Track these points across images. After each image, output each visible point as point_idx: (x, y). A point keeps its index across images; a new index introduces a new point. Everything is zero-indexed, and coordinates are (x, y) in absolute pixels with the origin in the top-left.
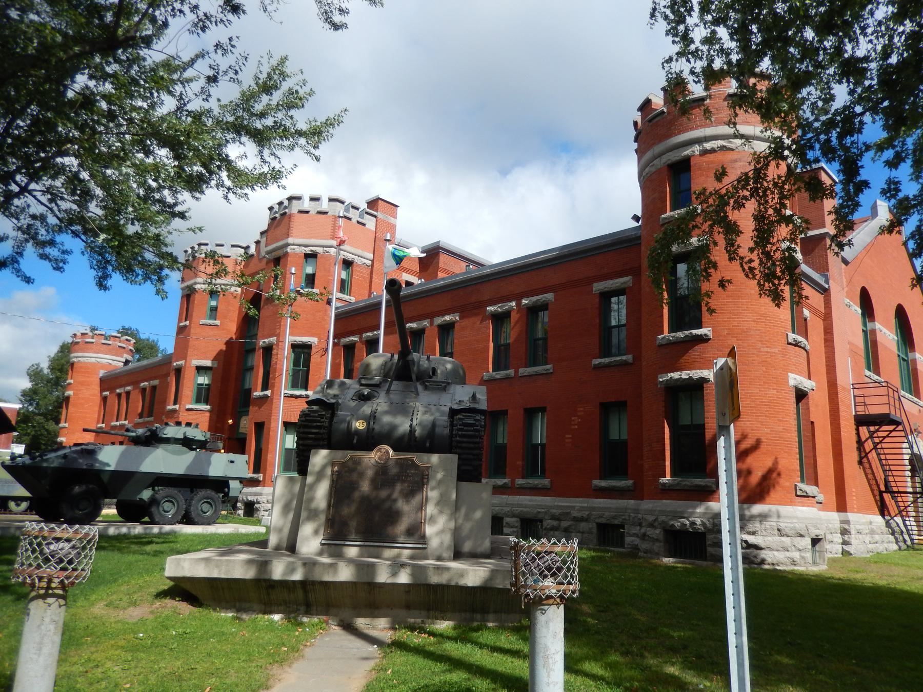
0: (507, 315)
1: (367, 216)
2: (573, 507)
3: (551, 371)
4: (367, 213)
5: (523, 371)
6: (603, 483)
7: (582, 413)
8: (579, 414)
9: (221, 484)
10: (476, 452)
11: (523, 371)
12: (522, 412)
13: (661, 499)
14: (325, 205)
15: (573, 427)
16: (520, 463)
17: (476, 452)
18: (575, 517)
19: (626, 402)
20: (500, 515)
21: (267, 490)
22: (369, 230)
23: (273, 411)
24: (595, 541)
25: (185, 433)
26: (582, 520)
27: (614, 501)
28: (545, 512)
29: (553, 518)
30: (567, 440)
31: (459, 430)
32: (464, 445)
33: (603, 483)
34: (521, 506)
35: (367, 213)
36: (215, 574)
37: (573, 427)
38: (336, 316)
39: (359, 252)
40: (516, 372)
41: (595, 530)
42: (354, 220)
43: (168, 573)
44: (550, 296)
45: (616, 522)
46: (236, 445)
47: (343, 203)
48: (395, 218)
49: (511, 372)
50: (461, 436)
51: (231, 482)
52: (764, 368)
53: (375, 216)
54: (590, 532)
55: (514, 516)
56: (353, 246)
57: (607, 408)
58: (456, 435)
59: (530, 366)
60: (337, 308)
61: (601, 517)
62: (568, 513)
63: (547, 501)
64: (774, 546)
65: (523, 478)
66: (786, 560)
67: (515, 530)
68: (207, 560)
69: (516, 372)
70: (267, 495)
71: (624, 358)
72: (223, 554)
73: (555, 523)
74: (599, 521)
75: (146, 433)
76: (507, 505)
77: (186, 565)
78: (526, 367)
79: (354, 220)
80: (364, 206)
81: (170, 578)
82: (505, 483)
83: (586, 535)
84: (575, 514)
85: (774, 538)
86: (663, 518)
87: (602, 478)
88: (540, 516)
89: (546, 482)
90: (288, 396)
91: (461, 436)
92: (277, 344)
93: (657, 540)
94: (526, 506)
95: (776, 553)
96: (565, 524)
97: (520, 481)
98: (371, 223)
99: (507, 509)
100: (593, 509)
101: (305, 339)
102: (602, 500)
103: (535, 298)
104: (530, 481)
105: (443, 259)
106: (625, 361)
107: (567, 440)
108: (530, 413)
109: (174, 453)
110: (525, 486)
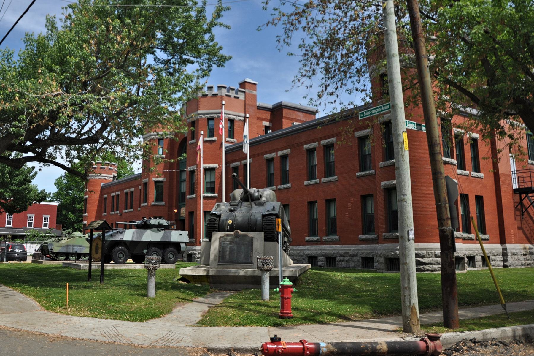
0: (314, 149)
1: (239, 93)
2: (350, 249)
3: (337, 179)
4: (240, 91)
5: (323, 180)
6: (364, 237)
7: (353, 201)
8: (351, 201)
9: (177, 245)
10: (272, 230)
11: (323, 180)
12: (324, 201)
13: (384, 243)
14: (215, 91)
15: (349, 209)
16: (324, 228)
17: (272, 230)
18: (351, 255)
19: (372, 194)
20: (316, 256)
21: (198, 247)
22: (241, 100)
23: (198, 205)
24: (361, 266)
25: (159, 223)
26: (354, 256)
27: (369, 245)
28: (337, 253)
29: (341, 255)
30: (346, 216)
31: (265, 222)
32: (267, 228)
33: (364, 237)
34: (325, 250)
35: (240, 91)
36: (194, 274)
37: (349, 209)
38: (225, 152)
39: (237, 114)
40: (320, 180)
41: (360, 261)
42: (232, 97)
43: (180, 274)
44: (334, 139)
45: (370, 256)
46: (181, 226)
47: (225, 88)
48: (256, 91)
49: (317, 180)
50: (266, 225)
51: (181, 244)
52: (428, 177)
53: (244, 92)
54: (358, 262)
55: (323, 256)
56: (233, 111)
57: (364, 198)
58: (264, 225)
59: (327, 177)
60: (226, 148)
61: (363, 254)
62: (348, 253)
63: (338, 247)
64: (433, 262)
65: (326, 236)
66: (439, 268)
67: (323, 262)
68: (192, 269)
69: (320, 180)
70: (198, 250)
71: (371, 172)
72: (197, 268)
73: (342, 258)
74: (362, 256)
75: (142, 223)
76: (319, 250)
77: (186, 271)
78: (325, 177)
79: (232, 97)
80: (237, 87)
81: (181, 275)
82: (318, 239)
83: (356, 263)
84: (351, 253)
85: (433, 258)
86: (384, 252)
87: (363, 234)
88: (335, 255)
89: (337, 237)
90: (204, 198)
91: (266, 225)
92: (197, 170)
93: (382, 263)
94: (328, 250)
95: (433, 265)
96: (346, 258)
97: (325, 238)
98: (242, 97)
99: (319, 252)
100: (360, 250)
101: (212, 166)
102: (363, 245)
103: (327, 141)
104: (330, 237)
105: (285, 112)
106: (371, 173)
107: (346, 216)
108: (329, 202)
109: (154, 231)
110: (327, 240)
